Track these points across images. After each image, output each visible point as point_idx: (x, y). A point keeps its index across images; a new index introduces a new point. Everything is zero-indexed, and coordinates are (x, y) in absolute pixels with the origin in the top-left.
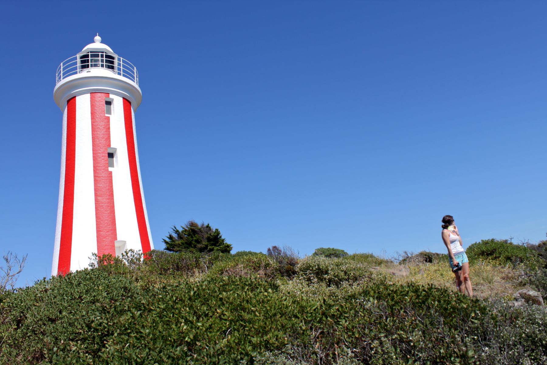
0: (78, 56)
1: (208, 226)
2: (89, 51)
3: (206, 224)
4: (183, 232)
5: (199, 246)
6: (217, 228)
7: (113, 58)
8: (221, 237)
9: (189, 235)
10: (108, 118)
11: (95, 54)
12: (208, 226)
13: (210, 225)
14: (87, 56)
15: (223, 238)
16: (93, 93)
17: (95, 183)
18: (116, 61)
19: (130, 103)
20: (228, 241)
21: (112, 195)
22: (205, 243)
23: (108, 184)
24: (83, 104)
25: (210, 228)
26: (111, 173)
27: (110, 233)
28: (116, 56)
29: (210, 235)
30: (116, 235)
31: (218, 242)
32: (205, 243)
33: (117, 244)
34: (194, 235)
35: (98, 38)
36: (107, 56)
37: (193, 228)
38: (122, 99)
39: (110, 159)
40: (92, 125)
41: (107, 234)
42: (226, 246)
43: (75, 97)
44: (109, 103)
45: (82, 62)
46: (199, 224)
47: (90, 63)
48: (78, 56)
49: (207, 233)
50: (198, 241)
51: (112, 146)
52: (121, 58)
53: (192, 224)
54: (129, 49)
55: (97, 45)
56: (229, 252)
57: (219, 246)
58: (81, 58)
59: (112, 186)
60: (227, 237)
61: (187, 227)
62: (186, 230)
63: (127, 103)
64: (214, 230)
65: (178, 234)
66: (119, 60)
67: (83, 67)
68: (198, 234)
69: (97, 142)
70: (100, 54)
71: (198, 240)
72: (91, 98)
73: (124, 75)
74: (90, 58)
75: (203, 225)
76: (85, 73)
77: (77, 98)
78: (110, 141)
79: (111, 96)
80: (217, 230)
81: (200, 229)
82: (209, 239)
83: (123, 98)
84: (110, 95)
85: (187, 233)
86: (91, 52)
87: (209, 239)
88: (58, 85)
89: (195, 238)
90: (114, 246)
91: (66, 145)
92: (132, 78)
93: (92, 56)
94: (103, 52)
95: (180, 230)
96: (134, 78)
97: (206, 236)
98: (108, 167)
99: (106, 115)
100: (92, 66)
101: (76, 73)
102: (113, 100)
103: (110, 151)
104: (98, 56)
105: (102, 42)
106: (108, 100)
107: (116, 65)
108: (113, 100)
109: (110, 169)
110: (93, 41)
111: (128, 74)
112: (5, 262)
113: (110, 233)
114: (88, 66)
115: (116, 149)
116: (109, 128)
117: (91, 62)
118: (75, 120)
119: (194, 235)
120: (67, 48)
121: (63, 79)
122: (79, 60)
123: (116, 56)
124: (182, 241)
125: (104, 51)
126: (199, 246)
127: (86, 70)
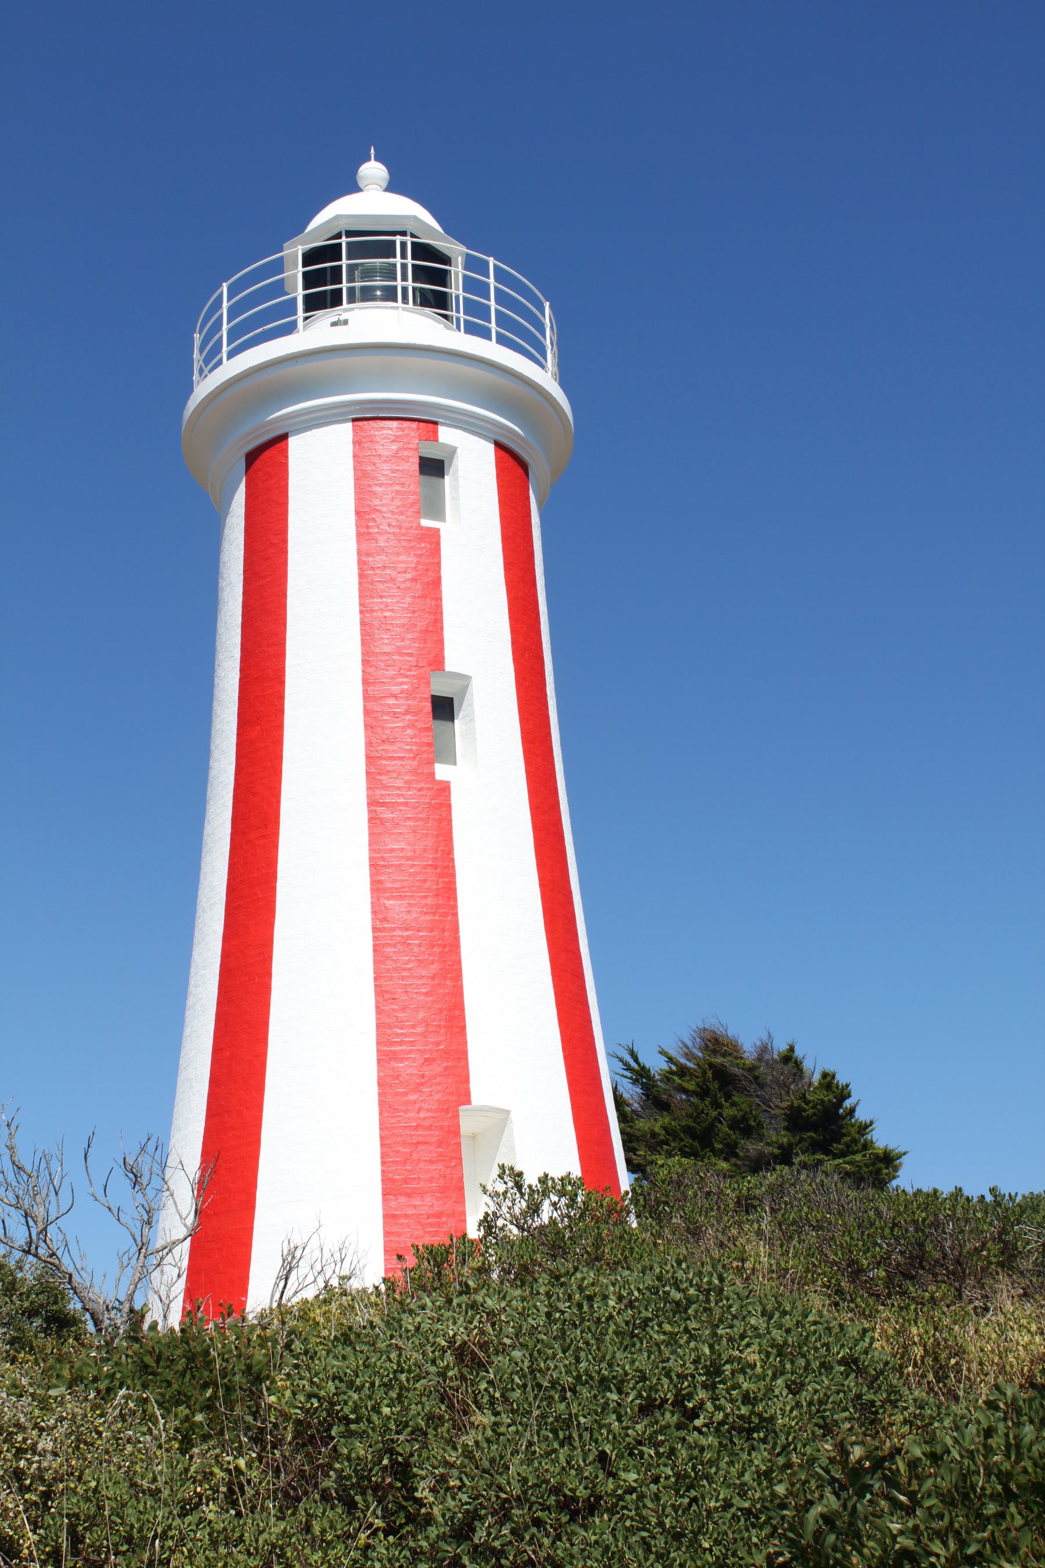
0: (296, 250)
1: (789, 1058)
2: (343, 226)
3: (780, 1046)
4: (667, 1077)
5: (752, 1147)
6: (830, 1068)
7: (446, 260)
8: (852, 1111)
9: (703, 1092)
10: (434, 536)
11: (373, 242)
12: (789, 1058)
13: (799, 1053)
14: (332, 252)
15: (862, 1115)
16: (363, 418)
17: (372, 834)
18: (457, 271)
19: (524, 466)
20: (881, 1139)
21: (448, 891)
22: (777, 1135)
23: (430, 842)
24: (321, 468)
25: (798, 1064)
26: (444, 789)
27: (437, 1068)
28: (456, 250)
29: (803, 1098)
30: (465, 1079)
31: (837, 1137)
32: (777, 1135)
33: (468, 1122)
34: (728, 1097)
35: (373, 171)
36: (422, 251)
37: (719, 1060)
38: (491, 447)
39: (440, 725)
40: (362, 564)
41: (428, 1071)
42: (877, 1157)
43: (284, 437)
44: (434, 467)
45: (310, 280)
46: (749, 1044)
47: (345, 285)
48: (296, 250)
49: (784, 1086)
50: (745, 1127)
51: (451, 664)
52: (491, 261)
53: (715, 1044)
54: (517, 219)
55: (373, 199)
56: (880, 1184)
57: (843, 1154)
58: (310, 257)
59: (449, 851)
60: (883, 1114)
61: (689, 1055)
62: (682, 1071)
63: (512, 464)
64: (816, 1078)
65: (646, 1087)
66: (470, 263)
67: (314, 303)
68: (743, 1090)
69: (385, 644)
70: (398, 239)
71: (744, 1118)
72: (356, 443)
73: (502, 340)
74: (344, 262)
75: (764, 1049)
76: (317, 332)
77: (293, 442)
78: (440, 642)
79: (447, 435)
80: (828, 1080)
81: (752, 1069)
82: (795, 1120)
83: (498, 445)
84: (441, 429)
85: (691, 1086)
86: (350, 234)
87: (795, 1120)
88: (204, 387)
89: (729, 1112)
90: (456, 1132)
91: (237, 654)
92: (535, 353)
93: (355, 251)
94: (403, 233)
95: (656, 1065)
96: (544, 355)
97: (783, 1103)
98: (431, 763)
99: (425, 523)
100: (352, 300)
101: (290, 329)
102: (453, 451)
103: (440, 687)
104: (387, 249)
105: (393, 187)
106: (430, 451)
107: (456, 289)
108: (453, 451)
109: (442, 772)
110: (355, 188)
111: (521, 336)
112: (128, 1184)
113: (437, 1068)
114: (335, 299)
115: (467, 678)
116: (437, 583)
117: (351, 280)
118: (285, 541)
119: (728, 1097)
120: (234, 220)
121: (231, 355)
122: (297, 272)
123: (456, 250)
124: (666, 1120)
125: (409, 227)
126: (752, 1147)
127: (325, 317)
